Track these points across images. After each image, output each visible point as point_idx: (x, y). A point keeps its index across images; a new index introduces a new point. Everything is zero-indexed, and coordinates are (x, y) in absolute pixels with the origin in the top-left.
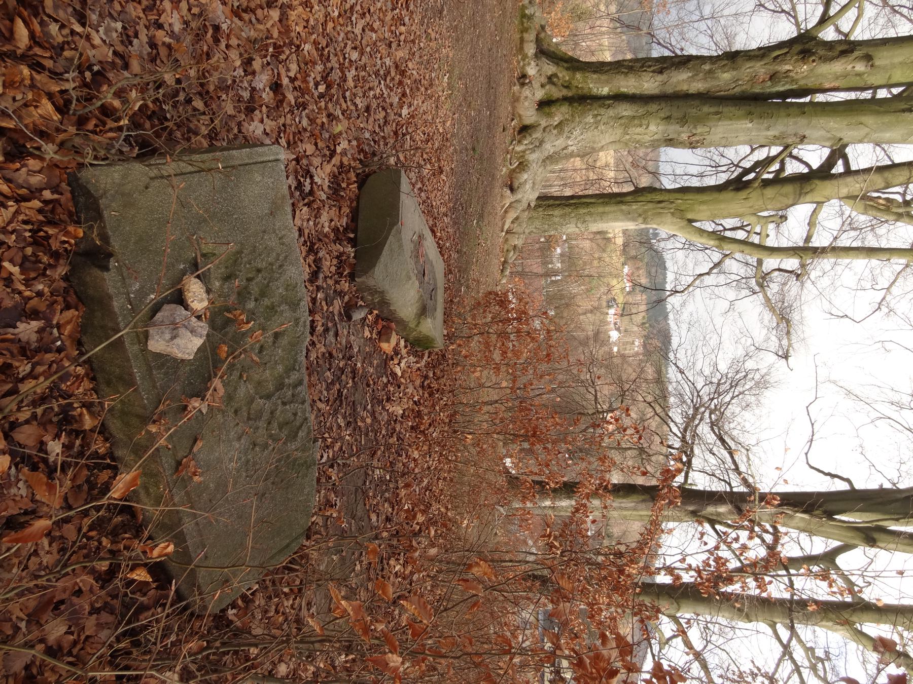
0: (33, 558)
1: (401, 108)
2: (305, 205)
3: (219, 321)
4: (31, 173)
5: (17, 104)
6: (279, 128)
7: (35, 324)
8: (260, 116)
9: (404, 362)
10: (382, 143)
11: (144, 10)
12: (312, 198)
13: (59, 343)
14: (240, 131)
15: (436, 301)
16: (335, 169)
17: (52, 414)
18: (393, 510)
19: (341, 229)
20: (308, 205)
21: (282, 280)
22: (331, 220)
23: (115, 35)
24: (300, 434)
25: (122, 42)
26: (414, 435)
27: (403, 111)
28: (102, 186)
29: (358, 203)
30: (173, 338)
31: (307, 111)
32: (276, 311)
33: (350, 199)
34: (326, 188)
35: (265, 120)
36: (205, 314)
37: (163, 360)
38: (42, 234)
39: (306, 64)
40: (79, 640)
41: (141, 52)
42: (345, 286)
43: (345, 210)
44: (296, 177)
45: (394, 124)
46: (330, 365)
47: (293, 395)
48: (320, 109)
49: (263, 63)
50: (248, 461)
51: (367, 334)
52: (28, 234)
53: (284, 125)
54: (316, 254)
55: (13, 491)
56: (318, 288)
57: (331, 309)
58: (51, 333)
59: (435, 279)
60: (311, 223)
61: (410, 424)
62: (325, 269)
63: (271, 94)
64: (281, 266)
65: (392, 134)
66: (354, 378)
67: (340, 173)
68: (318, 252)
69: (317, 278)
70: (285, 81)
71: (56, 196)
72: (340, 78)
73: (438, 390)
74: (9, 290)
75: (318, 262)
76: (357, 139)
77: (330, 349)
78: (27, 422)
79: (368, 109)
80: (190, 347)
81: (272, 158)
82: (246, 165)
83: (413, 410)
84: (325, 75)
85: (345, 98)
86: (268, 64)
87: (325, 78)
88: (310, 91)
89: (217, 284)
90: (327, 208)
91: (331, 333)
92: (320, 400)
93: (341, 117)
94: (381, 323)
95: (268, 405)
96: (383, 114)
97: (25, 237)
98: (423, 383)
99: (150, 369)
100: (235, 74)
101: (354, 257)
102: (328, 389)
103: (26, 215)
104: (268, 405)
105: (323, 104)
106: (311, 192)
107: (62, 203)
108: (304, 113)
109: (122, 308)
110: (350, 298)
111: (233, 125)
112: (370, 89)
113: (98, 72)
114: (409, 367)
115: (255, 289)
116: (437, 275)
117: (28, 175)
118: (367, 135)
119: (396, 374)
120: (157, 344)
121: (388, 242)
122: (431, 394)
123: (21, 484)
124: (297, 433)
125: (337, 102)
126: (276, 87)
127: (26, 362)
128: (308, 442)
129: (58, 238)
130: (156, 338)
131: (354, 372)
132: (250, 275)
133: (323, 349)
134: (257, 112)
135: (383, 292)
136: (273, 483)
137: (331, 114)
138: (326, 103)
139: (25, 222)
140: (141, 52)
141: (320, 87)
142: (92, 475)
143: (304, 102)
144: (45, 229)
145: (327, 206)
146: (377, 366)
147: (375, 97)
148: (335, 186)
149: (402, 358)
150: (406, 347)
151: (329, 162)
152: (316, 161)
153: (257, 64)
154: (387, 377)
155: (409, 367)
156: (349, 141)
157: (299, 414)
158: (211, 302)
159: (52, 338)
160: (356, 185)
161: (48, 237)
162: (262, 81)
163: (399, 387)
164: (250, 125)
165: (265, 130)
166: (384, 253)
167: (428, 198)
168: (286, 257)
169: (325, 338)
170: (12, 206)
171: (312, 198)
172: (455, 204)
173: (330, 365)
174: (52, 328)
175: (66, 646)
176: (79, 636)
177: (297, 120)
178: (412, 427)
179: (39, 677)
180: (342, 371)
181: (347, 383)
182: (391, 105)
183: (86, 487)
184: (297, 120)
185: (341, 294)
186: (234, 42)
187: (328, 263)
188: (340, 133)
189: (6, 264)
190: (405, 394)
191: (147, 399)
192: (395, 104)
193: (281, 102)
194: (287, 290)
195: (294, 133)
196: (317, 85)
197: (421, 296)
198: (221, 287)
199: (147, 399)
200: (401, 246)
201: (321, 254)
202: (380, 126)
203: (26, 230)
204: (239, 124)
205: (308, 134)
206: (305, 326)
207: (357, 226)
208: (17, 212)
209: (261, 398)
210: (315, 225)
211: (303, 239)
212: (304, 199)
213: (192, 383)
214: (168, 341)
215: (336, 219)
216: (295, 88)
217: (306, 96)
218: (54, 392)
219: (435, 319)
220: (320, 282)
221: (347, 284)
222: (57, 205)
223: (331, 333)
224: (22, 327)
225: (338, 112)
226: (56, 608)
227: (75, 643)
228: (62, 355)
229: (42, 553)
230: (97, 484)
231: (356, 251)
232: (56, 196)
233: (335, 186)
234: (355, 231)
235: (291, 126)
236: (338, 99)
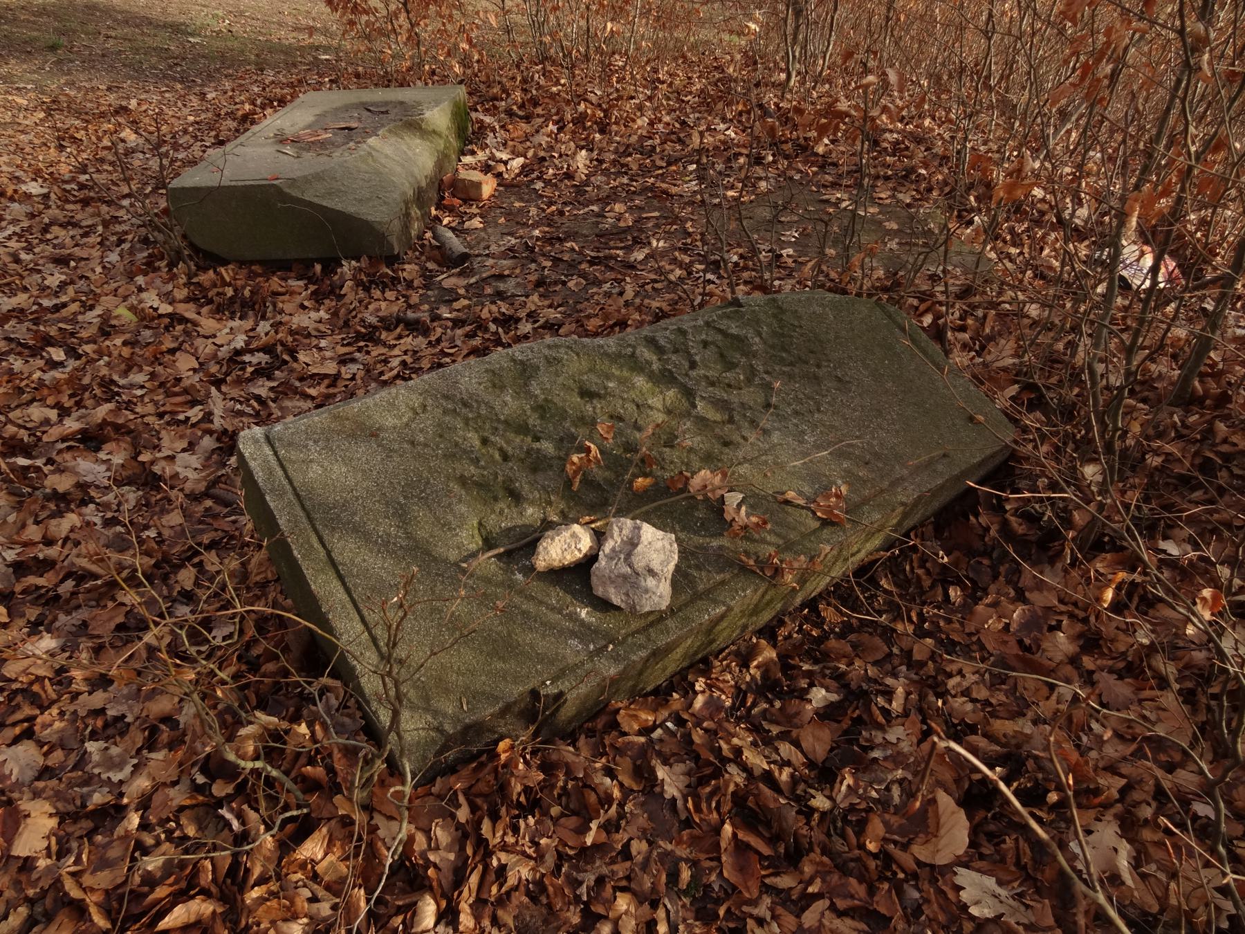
0: (974, 695)
1: (28, 196)
2: (296, 360)
3: (591, 497)
4: (434, 846)
5: (321, 893)
6: (168, 423)
7: (661, 773)
8: (163, 463)
9: (499, 155)
10: (119, 228)
11: (43, 709)
12: (279, 348)
13: (669, 724)
14: (206, 494)
15: (386, 103)
16: (205, 310)
17: (773, 710)
18: (741, 154)
19: (312, 288)
20: (293, 352)
21: (487, 398)
22: (303, 307)
23: (115, 751)
24: (734, 331)
25: (122, 734)
26: (614, 127)
27: (34, 191)
28: (422, 733)
29: (252, 263)
30: (651, 572)
31: (116, 377)
32: (546, 400)
33: (249, 278)
34: (249, 324)
35: (165, 453)
36: (587, 523)
37: (680, 579)
38: (522, 799)
39: (20, 391)
40: (1068, 612)
41: (128, 697)
42: (410, 270)
43: (275, 283)
44: (249, 380)
45: (70, 207)
46: (556, 283)
47: (676, 351)
48: (100, 354)
49: (53, 472)
50: (796, 413)
51: (476, 223)
52: (531, 820)
53: (161, 416)
54: (375, 328)
55: (905, 747)
56: (436, 318)
57: (462, 291)
58: (661, 740)
59: (347, 108)
60: (323, 343)
61: (597, 135)
62: (395, 309)
63: (108, 447)
64: (465, 404)
65: (90, 210)
66: (559, 239)
67: (210, 302)
68: (370, 326)
69: (417, 321)
70: (72, 425)
71: (462, 799)
72: (20, 321)
73: (525, 91)
74: (623, 823)
75: (388, 323)
76: (131, 277)
77: (530, 286)
78: (797, 744)
79: (61, 261)
80: (660, 544)
81: (267, 450)
82: (297, 495)
83: (573, 132)
84: (26, 352)
85: (57, 308)
86: (50, 461)
87: (35, 352)
88: (71, 375)
89: (530, 511)
90: (285, 318)
91: (502, 286)
92: (621, 294)
93: (98, 311)
94: (448, 199)
95: (704, 391)
96: (56, 230)
97: (536, 823)
98: (521, 118)
99: (697, 597)
100: (97, 520)
101: (358, 261)
102: (598, 283)
103: (505, 834)
104: (704, 391)
105: (88, 348)
106: (268, 349)
107: (466, 785)
108: (122, 382)
109: (616, 658)
110: (429, 259)
111: (199, 509)
112: (17, 260)
113: (204, 771)
114: (505, 144)
115: (517, 443)
116: (338, 104)
117: (437, 848)
118: (113, 257)
119: (523, 166)
120: (659, 593)
121: (316, 200)
122: (536, 104)
123: (892, 737)
124: (733, 337)
125: (73, 320)
126: (91, 440)
127: (727, 776)
128: (742, 317)
129: (524, 776)
130: (656, 599)
131: (549, 240)
132: (497, 456)
133: (535, 297)
134: (157, 469)
135: (406, 203)
136: (819, 366)
137: (101, 329)
138: (82, 341)
139: (515, 829)
140: (128, 697)
141: (55, 358)
142: (832, 631)
143: (100, 385)
144: (515, 798)
145: (278, 318)
146: (521, 200)
147: (29, 249)
148: (237, 306)
149: (492, 158)
150: (473, 153)
151: (195, 324)
152: (206, 348)
153: (63, 483)
154: (532, 181)
155: (505, 144)
156: (140, 290)
157: (704, 337)
158: (567, 520)
159: (666, 737)
160: (222, 270)
161: (527, 790)
162: (89, 468)
163: (544, 159)
164: (186, 479)
165: (184, 450)
166: (339, 207)
167: (185, 132)
168: (446, 397)
169: (514, 296)
170: (499, 860)
171: (279, 348)
172: (175, 79)
173: (556, 283)
174: (651, 741)
175: (1079, 627)
176: (1061, 613)
177: (139, 392)
178: (602, 132)
179: (1130, 659)
180: (556, 261)
181: (573, 249)
182: (32, 216)
183: (852, 637)
184: (139, 392)
185: (428, 278)
186: (33, 532)
187: (383, 305)
188: (132, 309)
189: (589, 841)
190: (551, 148)
191: (744, 590)
192: (29, 209)
193: (117, 428)
194: (502, 388)
195: (169, 394)
196: (53, 365)
197: (390, 131)
198: (532, 503)
199: (744, 590)
200: (318, 177)
201: (372, 320)
202: (86, 235)
203: (527, 825)
204: (195, 497)
205: (159, 369)
206: (557, 346)
207: (296, 260)
208: (504, 847)
209: (695, 406)
210: (322, 336)
211: (357, 355)
212: (286, 362)
213: (702, 524)
214: (659, 581)
215: (298, 299)
216: (79, 405)
217: (86, 381)
218: (740, 712)
219: (419, 104)
220: (423, 315)
221: (406, 266)
222: (473, 790)
223: (502, 286)
224: (671, 791)
225: (93, 316)
226: (1028, 649)
227: (1072, 616)
228: (685, 716)
229: (965, 684)
230: (843, 622)
231: (346, 258)
232: (462, 799)
233: (237, 306)
234: (309, 264)
235: (156, 403)
236: (64, 320)
